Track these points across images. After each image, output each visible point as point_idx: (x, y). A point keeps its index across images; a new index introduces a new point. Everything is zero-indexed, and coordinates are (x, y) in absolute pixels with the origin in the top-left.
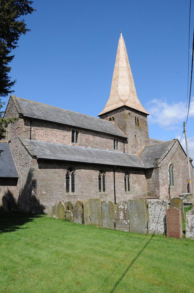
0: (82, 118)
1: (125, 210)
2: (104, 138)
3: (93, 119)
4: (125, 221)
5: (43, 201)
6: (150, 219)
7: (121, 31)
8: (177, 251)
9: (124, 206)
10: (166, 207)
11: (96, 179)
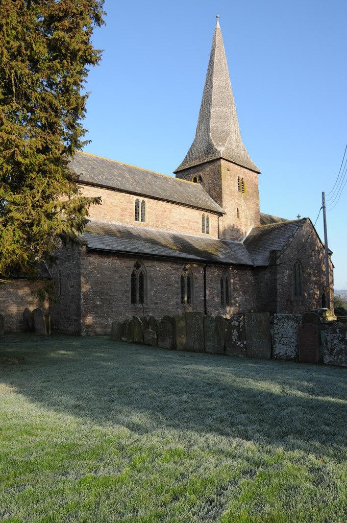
0: (150, 177)
1: (241, 327)
2: (340, 290)
3: (166, 179)
4: (239, 343)
5: (98, 317)
6: (276, 339)
7: (218, 16)
8: (251, 471)
9: (239, 323)
10: (299, 324)
11: (177, 282)
